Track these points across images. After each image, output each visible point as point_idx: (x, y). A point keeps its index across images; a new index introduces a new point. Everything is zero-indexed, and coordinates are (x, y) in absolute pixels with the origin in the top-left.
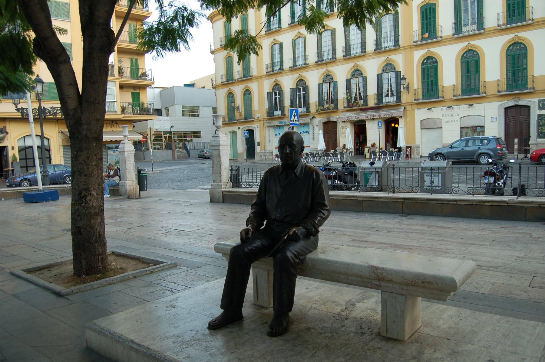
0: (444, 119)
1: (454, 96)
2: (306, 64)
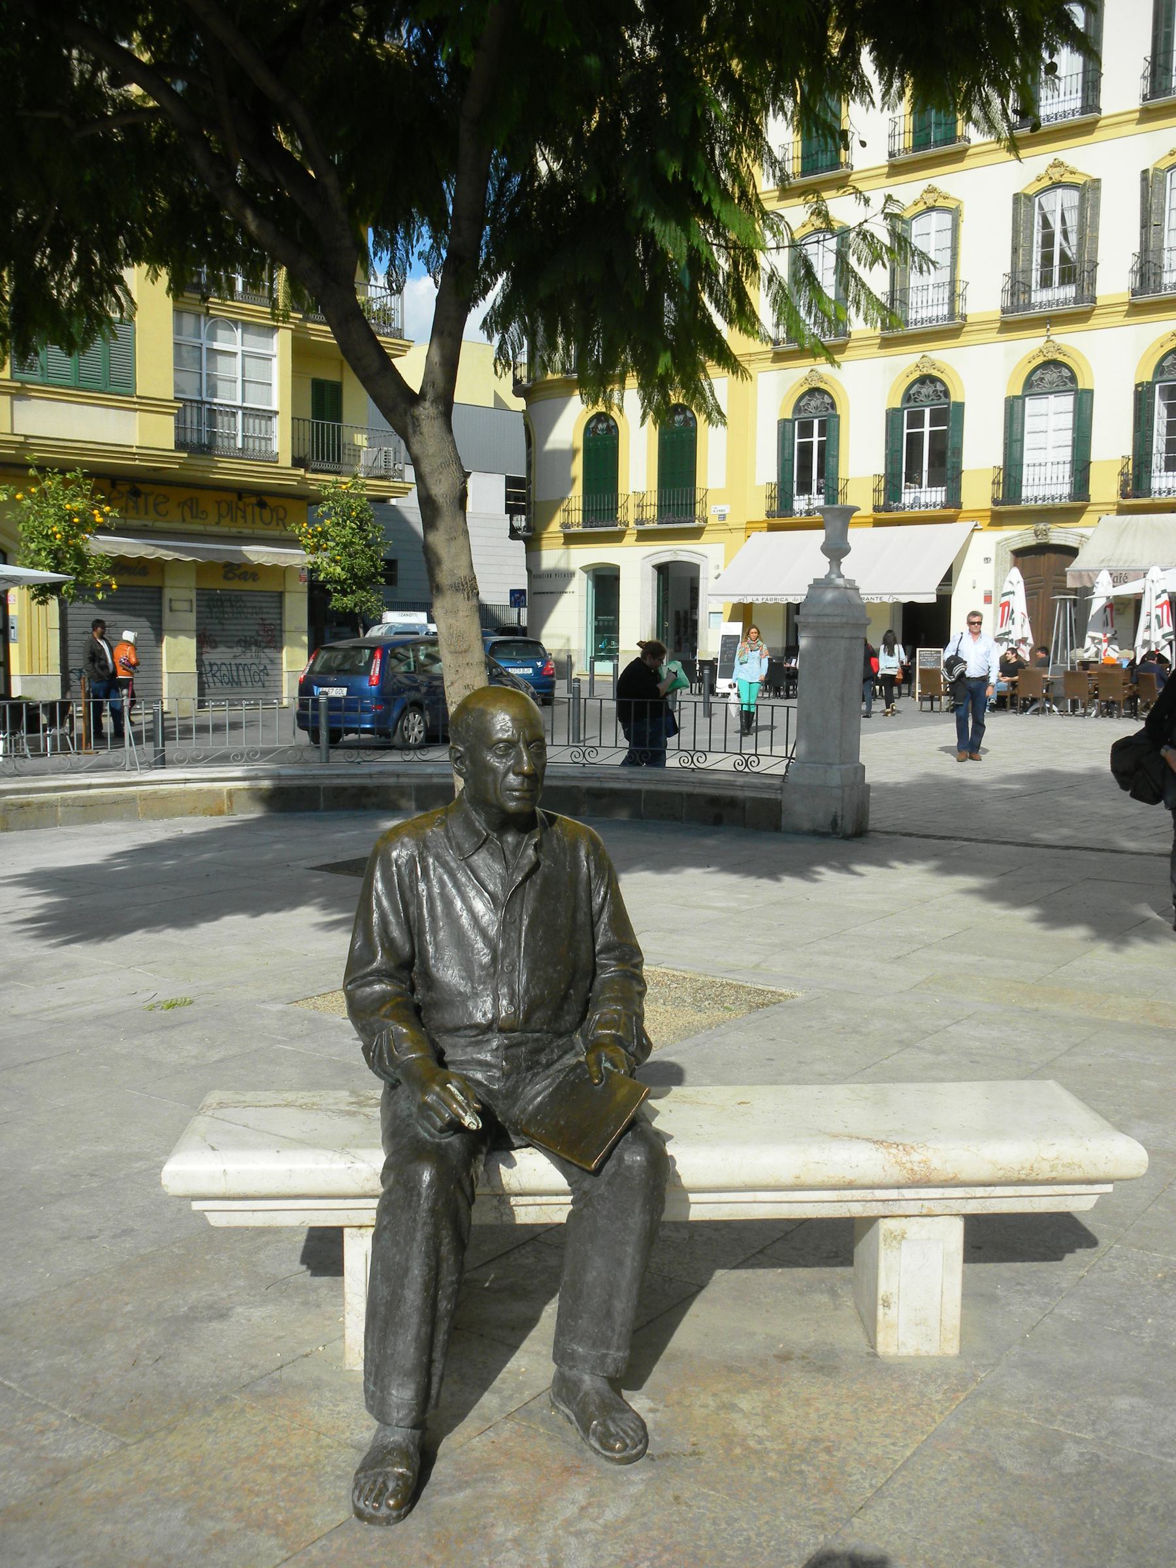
2: (952, 315)
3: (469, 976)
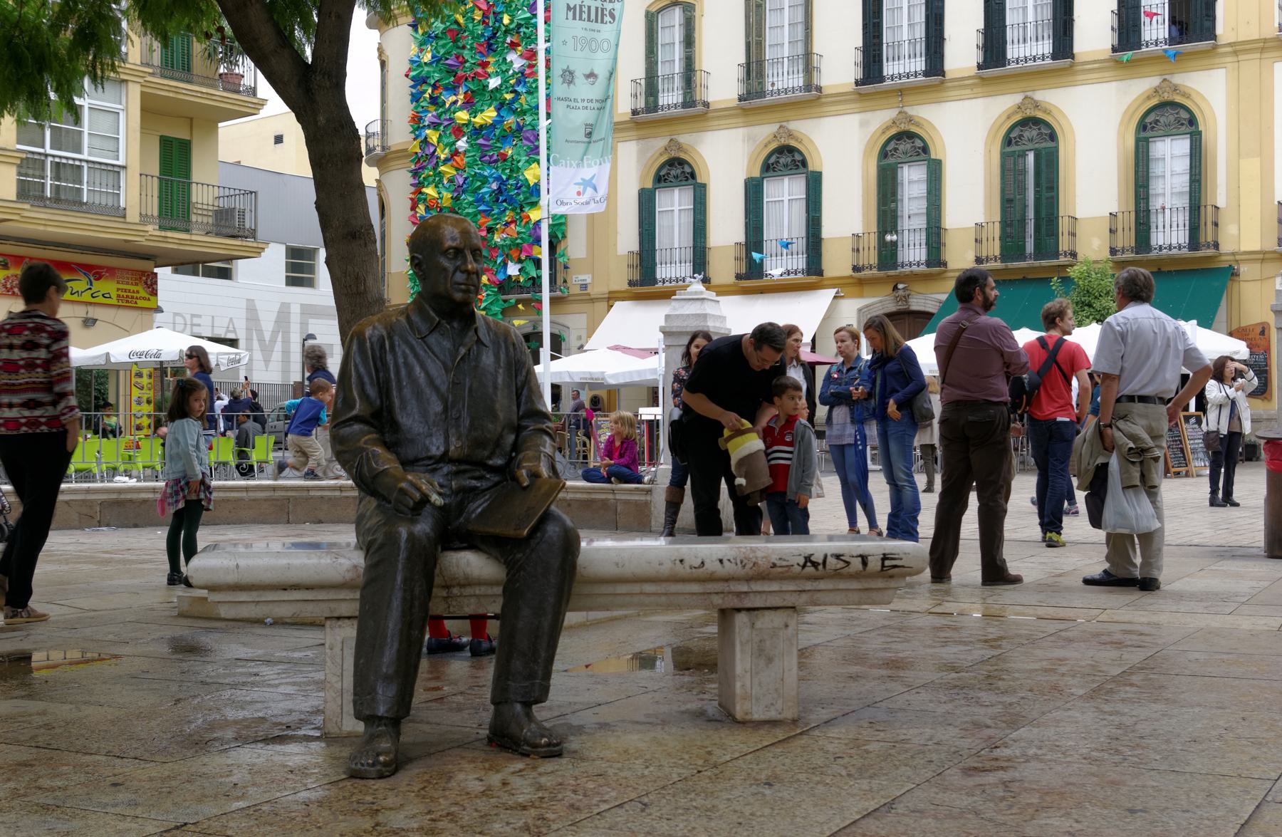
2: (808, 86)
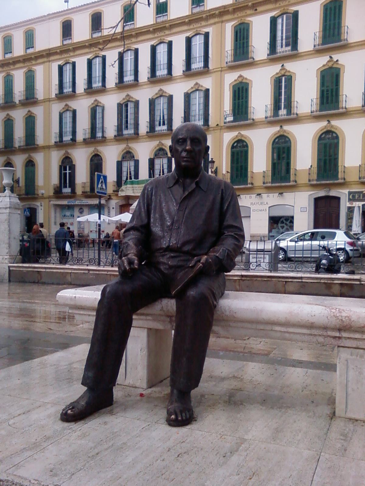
0: (252, 208)
1: (264, 183)
3: (163, 230)
